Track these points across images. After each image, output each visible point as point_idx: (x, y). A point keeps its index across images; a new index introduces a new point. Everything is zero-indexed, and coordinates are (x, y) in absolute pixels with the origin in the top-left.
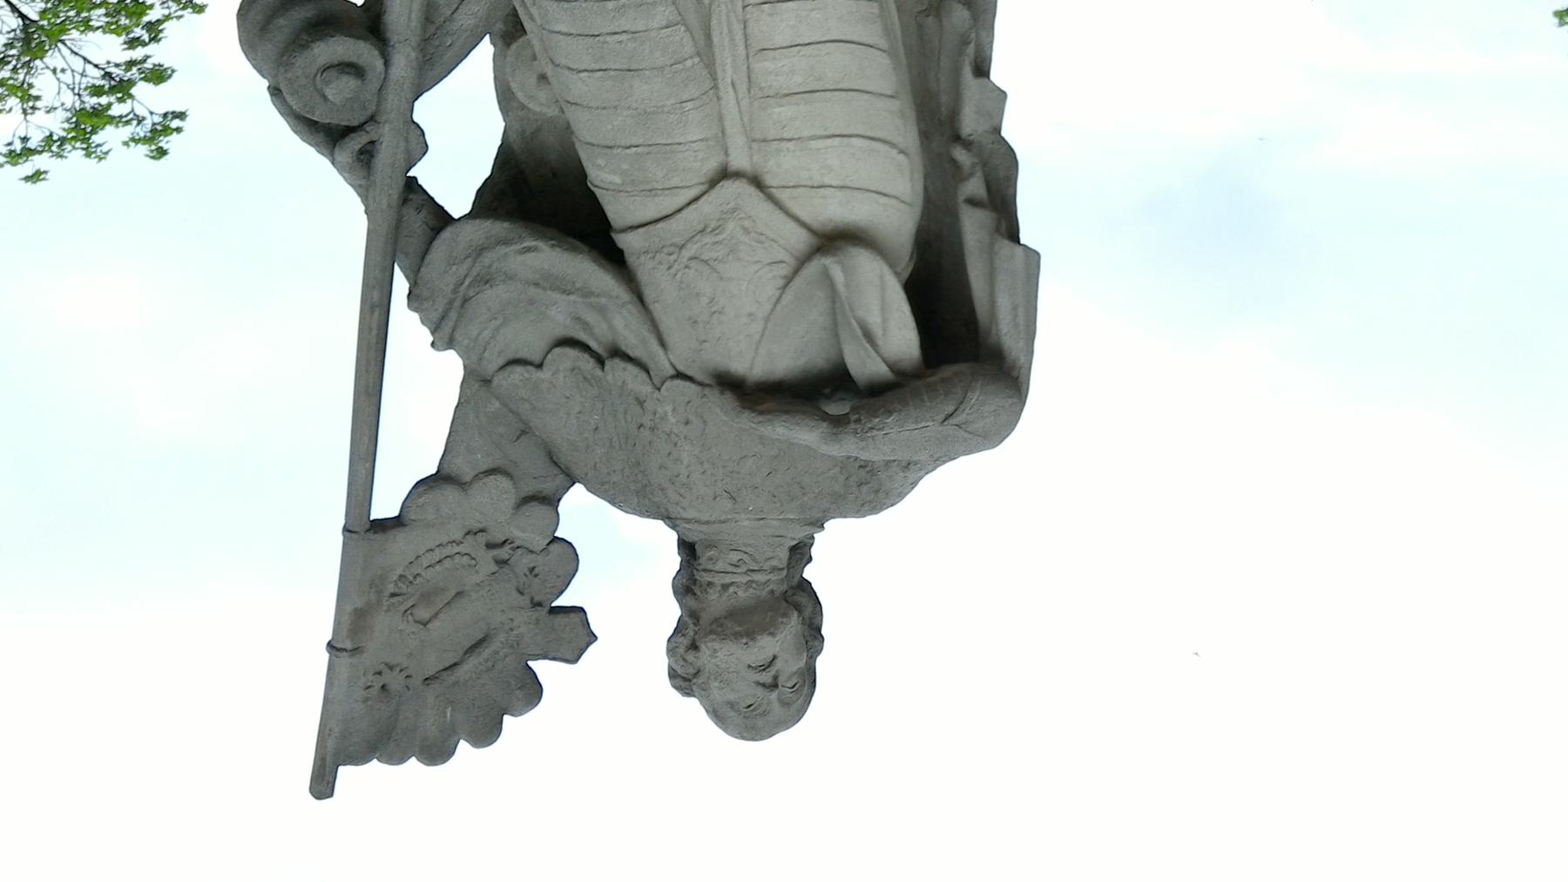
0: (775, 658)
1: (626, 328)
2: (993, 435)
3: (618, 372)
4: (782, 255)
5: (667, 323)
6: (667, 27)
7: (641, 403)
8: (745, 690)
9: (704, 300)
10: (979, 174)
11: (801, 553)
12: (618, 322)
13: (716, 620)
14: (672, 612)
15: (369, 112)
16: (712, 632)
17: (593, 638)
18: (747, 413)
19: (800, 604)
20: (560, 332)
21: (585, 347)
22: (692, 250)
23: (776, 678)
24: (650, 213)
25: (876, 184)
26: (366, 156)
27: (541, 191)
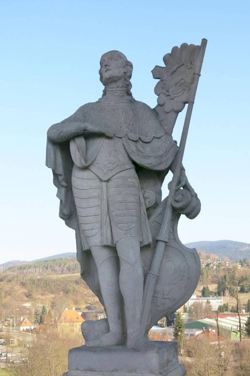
0: (106, 72)
1: (132, 147)
2: (54, 127)
3: (135, 137)
4: (96, 165)
5: (122, 150)
6: (113, 211)
7: (131, 131)
8: (113, 64)
9: (112, 155)
10: (60, 181)
11: (105, 92)
12: (134, 149)
13: (120, 80)
14: (132, 81)
15: (177, 192)
16: (120, 77)
17: (152, 72)
18: (103, 132)
19: (106, 81)
20: (149, 145)
21: (143, 142)
22: (114, 166)
23: (106, 67)
24: (123, 173)
25: (79, 179)
26: (179, 182)
27: (148, 175)
